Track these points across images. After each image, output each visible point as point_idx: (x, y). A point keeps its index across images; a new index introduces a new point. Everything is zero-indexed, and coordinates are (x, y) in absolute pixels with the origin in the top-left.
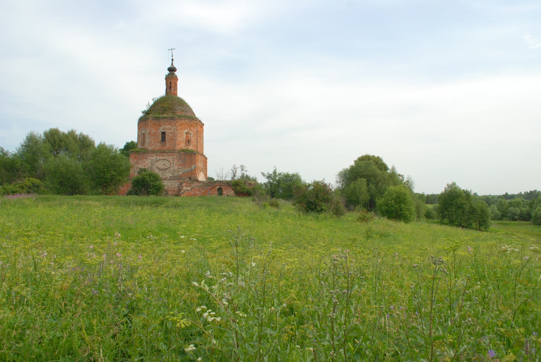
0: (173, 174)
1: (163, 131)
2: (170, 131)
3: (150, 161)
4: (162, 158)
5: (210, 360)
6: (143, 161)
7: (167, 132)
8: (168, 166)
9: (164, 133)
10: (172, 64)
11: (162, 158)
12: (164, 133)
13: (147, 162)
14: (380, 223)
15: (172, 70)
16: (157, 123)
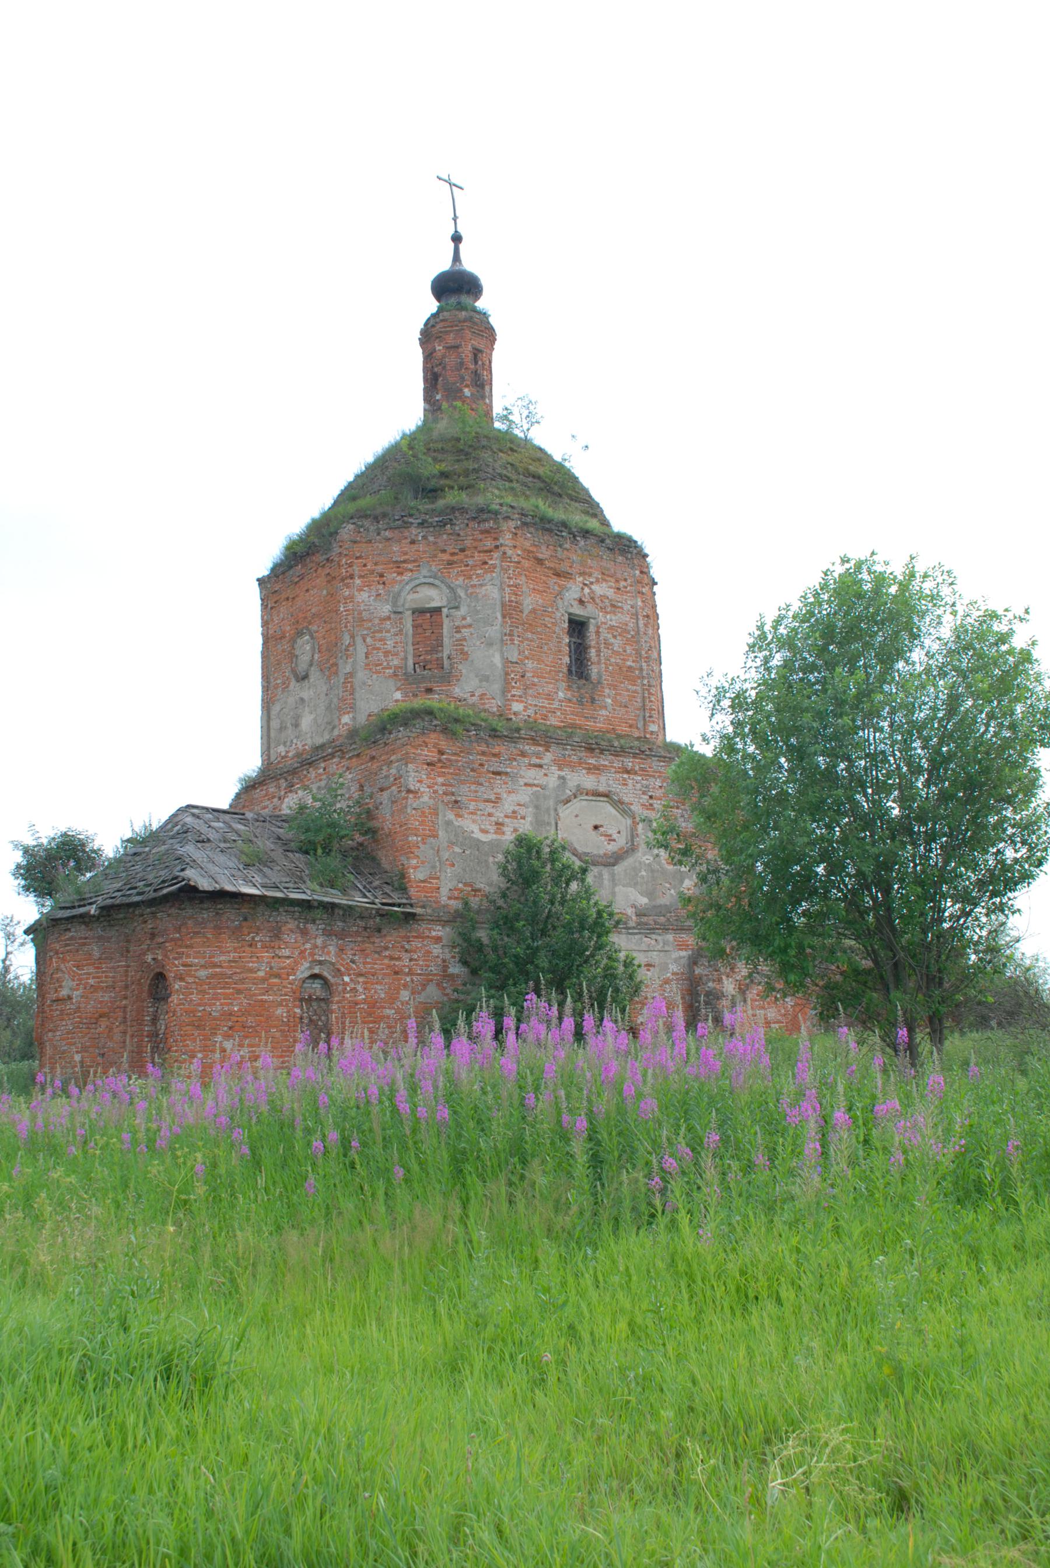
0: (650, 895)
1: (577, 610)
2: (613, 620)
3: (524, 795)
4: (589, 782)
5: (127, 1565)
6: (485, 793)
7: (601, 621)
8: (621, 841)
9: (577, 626)
10: (456, 258)
11: (589, 782)
12: (577, 626)
13: (509, 804)
14: (392, 937)
15: (456, 287)
16: (544, 553)
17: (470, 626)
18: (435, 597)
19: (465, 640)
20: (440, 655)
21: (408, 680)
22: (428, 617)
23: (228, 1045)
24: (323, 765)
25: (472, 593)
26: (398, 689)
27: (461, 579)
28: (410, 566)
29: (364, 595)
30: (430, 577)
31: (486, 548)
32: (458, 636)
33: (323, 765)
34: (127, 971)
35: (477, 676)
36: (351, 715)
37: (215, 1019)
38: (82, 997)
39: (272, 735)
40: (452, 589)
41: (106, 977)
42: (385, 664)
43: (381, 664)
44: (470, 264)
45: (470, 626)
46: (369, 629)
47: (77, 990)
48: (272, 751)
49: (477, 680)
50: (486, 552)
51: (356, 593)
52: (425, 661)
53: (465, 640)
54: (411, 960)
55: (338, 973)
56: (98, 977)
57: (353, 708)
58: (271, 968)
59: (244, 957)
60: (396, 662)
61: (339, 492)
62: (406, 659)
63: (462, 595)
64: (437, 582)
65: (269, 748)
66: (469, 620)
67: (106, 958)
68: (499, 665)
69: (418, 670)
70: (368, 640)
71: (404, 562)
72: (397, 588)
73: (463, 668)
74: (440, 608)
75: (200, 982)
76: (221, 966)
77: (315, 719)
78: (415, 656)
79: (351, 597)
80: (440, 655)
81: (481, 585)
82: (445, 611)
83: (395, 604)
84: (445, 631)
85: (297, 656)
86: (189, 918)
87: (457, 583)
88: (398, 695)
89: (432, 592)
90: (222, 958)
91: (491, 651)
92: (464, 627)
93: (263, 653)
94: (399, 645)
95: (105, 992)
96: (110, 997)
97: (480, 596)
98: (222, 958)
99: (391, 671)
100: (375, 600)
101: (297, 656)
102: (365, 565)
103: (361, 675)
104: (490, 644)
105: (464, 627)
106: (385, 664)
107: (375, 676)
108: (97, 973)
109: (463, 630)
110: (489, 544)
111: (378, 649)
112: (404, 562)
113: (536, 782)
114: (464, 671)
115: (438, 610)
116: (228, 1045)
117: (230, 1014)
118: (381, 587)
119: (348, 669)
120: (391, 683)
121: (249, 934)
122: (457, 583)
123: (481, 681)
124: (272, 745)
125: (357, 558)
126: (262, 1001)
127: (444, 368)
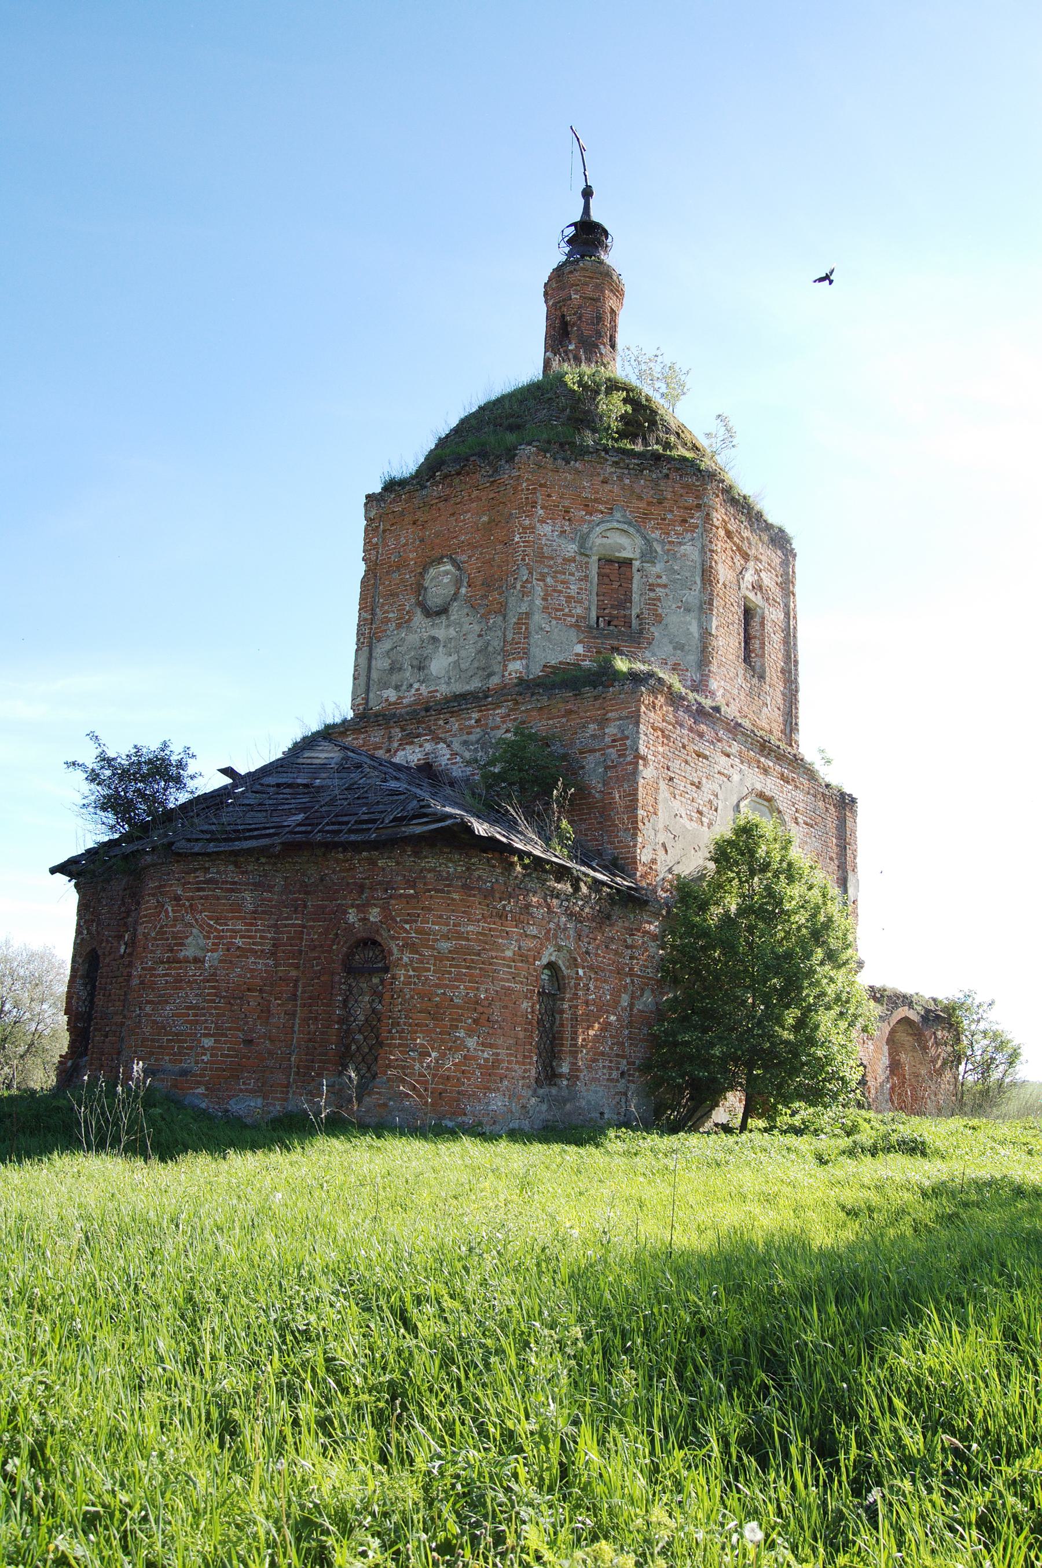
15: (588, 236)
17: (665, 586)
18: (627, 546)
19: (659, 600)
20: (628, 612)
21: (591, 632)
22: (616, 570)
23: (471, 1043)
24: (475, 715)
25: (669, 550)
26: (580, 642)
27: (658, 532)
28: (601, 507)
29: (547, 529)
30: (625, 523)
31: (686, 504)
32: (652, 595)
33: (475, 715)
34: (302, 932)
35: (670, 642)
36: (524, 662)
37: (458, 1007)
38: (221, 961)
39: (374, 675)
40: (648, 540)
41: (261, 937)
42: (567, 610)
43: (562, 610)
44: (596, 216)
45: (665, 586)
46: (551, 567)
47: (212, 951)
48: (371, 695)
49: (671, 647)
50: (686, 508)
51: (538, 525)
52: (610, 615)
53: (659, 600)
54: (632, 958)
55: (574, 963)
56: (249, 937)
57: (526, 654)
58: (520, 948)
59: (494, 930)
60: (579, 611)
61: (454, 422)
62: (589, 609)
63: (659, 549)
64: (631, 530)
65: (367, 691)
66: (664, 580)
67: (264, 912)
68: (696, 635)
69: (602, 625)
70: (549, 580)
71: (596, 500)
72: (585, 528)
73: (656, 631)
74: (631, 560)
75: (439, 958)
76: (468, 940)
77: (457, 663)
78: (598, 607)
79: (533, 528)
80: (628, 612)
81: (680, 544)
82: (636, 564)
83: (582, 546)
84: (635, 587)
85: (426, 589)
86: (429, 871)
87: (653, 535)
88: (579, 649)
89: (623, 540)
90: (470, 928)
91: (688, 618)
92: (659, 585)
93: (364, 582)
94: (583, 594)
95: (259, 957)
96: (266, 965)
97: (678, 555)
98: (470, 928)
99: (574, 620)
100: (559, 536)
101: (426, 589)
102: (549, 496)
103: (538, 618)
104: (688, 610)
105: (659, 585)
106: (567, 610)
107: (554, 622)
108: (248, 931)
109: (657, 590)
110: (691, 501)
111: (560, 592)
112: (596, 500)
113: (726, 772)
114: (656, 634)
115: (627, 563)
116: (471, 1043)
117: (477, 1003)
118: (567, 523)
119: (524, 608)
120: (573, 634)
121: (501, 900)
122: (653, 535)
123: (675, 648)
124: (374, 688)
125: (541, 486)
126: (509, 988)
127: (580, 318)
